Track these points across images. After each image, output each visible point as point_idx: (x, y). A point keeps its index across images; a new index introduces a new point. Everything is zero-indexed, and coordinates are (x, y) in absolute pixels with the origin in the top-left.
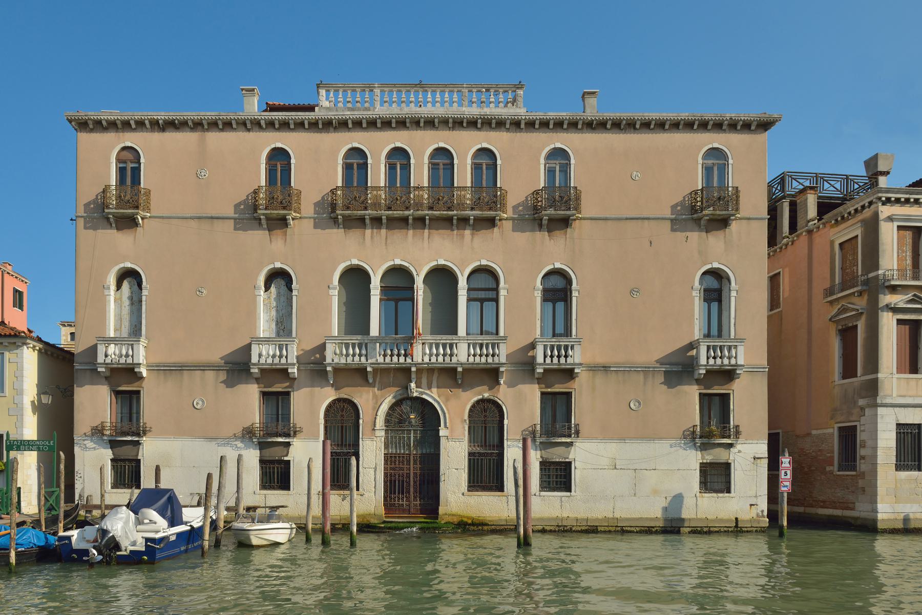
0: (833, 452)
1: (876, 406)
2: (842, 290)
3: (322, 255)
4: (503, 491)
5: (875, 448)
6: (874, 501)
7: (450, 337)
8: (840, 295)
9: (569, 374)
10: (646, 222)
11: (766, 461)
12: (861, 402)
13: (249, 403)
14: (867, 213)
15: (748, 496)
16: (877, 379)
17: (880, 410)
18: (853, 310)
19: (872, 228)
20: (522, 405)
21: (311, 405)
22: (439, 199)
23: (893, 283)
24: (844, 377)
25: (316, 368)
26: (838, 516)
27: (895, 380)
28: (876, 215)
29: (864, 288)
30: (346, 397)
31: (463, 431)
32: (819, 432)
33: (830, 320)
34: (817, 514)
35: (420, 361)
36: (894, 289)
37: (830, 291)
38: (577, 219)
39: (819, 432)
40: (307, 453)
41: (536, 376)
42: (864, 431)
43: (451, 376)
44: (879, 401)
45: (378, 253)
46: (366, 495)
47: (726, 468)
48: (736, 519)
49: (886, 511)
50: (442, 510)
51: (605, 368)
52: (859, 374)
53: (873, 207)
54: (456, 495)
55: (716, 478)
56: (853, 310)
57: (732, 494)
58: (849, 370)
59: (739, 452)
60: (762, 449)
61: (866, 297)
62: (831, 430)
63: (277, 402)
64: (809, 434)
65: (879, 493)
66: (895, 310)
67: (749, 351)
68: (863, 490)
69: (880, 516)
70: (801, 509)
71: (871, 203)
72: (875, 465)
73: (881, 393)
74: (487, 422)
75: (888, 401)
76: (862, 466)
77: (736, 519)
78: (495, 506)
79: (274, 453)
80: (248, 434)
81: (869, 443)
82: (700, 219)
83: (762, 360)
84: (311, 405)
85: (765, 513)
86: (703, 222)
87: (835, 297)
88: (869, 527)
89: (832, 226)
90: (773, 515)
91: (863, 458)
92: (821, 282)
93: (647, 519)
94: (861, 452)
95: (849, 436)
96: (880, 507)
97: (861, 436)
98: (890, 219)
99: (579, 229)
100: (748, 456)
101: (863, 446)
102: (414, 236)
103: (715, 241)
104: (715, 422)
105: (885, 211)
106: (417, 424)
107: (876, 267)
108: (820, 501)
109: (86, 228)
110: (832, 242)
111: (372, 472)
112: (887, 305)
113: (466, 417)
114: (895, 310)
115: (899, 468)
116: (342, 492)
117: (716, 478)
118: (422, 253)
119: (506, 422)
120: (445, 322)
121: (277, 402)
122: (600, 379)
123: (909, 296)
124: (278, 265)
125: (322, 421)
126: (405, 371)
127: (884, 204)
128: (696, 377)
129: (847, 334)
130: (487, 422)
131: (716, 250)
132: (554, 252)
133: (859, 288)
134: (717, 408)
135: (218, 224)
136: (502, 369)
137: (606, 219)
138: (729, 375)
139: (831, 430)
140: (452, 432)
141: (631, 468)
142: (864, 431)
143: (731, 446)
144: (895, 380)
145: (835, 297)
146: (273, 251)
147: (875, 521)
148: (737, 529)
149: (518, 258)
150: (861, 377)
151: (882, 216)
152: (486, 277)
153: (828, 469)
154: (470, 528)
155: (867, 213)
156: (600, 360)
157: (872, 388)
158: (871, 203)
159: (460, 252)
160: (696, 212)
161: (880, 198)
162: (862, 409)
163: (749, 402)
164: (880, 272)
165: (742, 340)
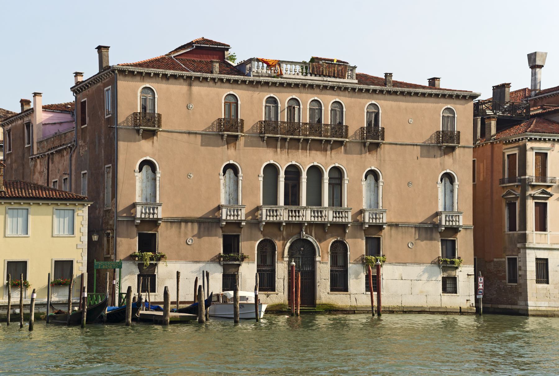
0: (505, 272)
1: (525, 248)
2: (509, 183)
3: (255, 159)
4: (347, 291)
5: (526, 271)
6: (526, 300)
7: (273, 206)
8: (507, 185)
9: (380, 228)
10: (415, 147)
11: (473, 277)
12: (519, 245)
13: (216, 245)
14: (521, 143)
15: (466, 294)
16: (526, 233)
17: (528, 251)
18: (514, 194)
19: (523, 151)
20: (357, 247)
21: (250, 247)
22: (233, 125)
23: (532, 183)
24: (510, 230)
25: (254, 222)
26: (509, 309)
27: (534, 234)
28: (525, 146)
29: (519, 184)
30: (269, 238)
31: (328, 259)
32: (498, 260)
33: (503, 197)
34: (498, 308)
35: (310, 220)
36: (533, 186)
37: (502, 181)
38: (384, 144)
39: (498, 260)
40: (248, 272)
41: (364, 228)
42: (520, 261)
43: (322, 228)
44: (527, 246)
45: (283, 160)
46: (279, 294)
47: (454, 279)
48: (460, 308)
49: (532, 304)
50: (318, 302)
51: (397, 225)
52: (517, 230)
53: (524, 141)
54: (324, 294)
55: (450, 285)
56: (514, 194)
57: (458, 294)
58: (512, 227)
59: (461, 271)
60: (471, 270)
61: (520, 189)
62: (504, 259)
63: (231, 245)
64: (493, 261)
65: (528, 295)
66: (534, 198)
67: (465, 220)
68: (521, 293)
69: (530, 308)
70: (489, 306)
71: (523, 139)
72: (526, 279)
73: (528, 241)
74: (339, 253)
75: (531, 246)
76: (520, 281)
77: (460, 308)
78: (339, 300)
79: (231, 271)
80: (217, 259)
81: (523, 268)
82: (441, 146)
83: (470, 223)
84: (250, 247)
85: (474, 305)
86: (442, 148)
87: (505, 185)
88: (525, 314)
89: (504, 144)
90: (477, 307)
91: (520, 276)
92: (498, 176)
93: (417, 307)
94: (520, 273)
95: (513, 262)
96: (530, 303)
97: (519, 264)
98: (532, 149)
99: (385, 149)
100: (465, 274)
101: (520, 270)
102: (302, 152)
103: (448, 159)
104: (448, 262)
105: (529, 145)
106: (304, 254)
107: (525, 174)
108: (502, 299)
109: (245, 146)
110: (504, 153)
111: (282, 281)
112: (530, 195)
113: (329, 250)
114: (534, 198)
115: (538, 282)
116: (266, 292)
117: (450, 285)
118: (305, 160)
119: (349, 253)
120: (315, 199)
121: (231, 245)
122: (394, 230)
123: (539, 191)
124: (232, 162)
125: (256, 252)
126: (300, 225)
127: (529, 141)
128: (440, 231)
129: (511, 206)
130: (339, 253)
131: (449, 164)
132: (371, 162)
133: (517, 184)
134: (450, 248)
135: (467, 150)
136: (349, 225)
137: (396, 144)
138: (455, 230)
139: (504, 259)
140: (322, 258)
141: (410, 281)
142: (520, 261)
143: (457, 268)
144: (534, 234)
145: (505, 185)
146: (230, 155)
147: (527, 310)
148: (461, 312)
149: (353, 165)
150: (518, 232)
151: (528, 147)
152: (337, 174)
153: (503, 281)
154: (330, 310)
155: (521, 143)
156: (394, 220)
157: (524, 238)
158: (523, 139)
159: (326, 161)
160: (439, 143)
161: (527, 138)
162: (519, 249)
163: (465, 244)
164: (527, 177)
165: (461, 213)
